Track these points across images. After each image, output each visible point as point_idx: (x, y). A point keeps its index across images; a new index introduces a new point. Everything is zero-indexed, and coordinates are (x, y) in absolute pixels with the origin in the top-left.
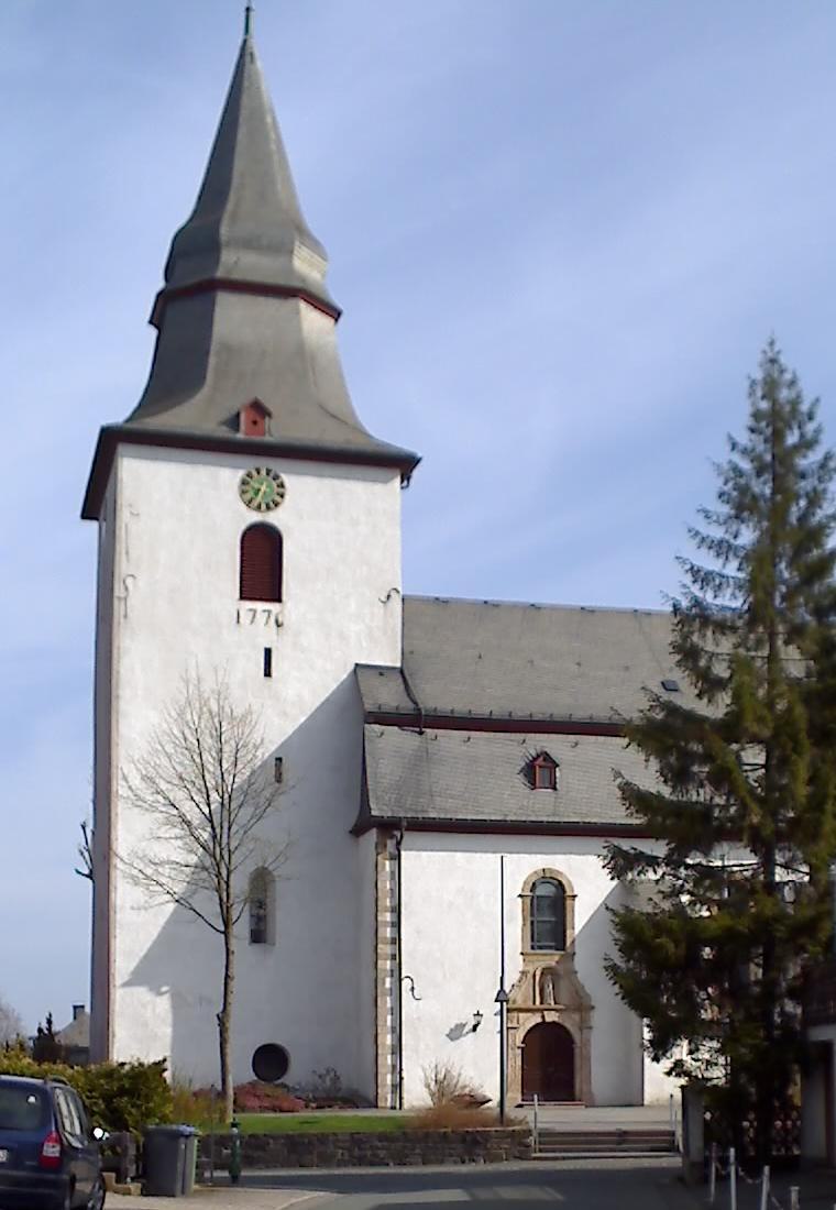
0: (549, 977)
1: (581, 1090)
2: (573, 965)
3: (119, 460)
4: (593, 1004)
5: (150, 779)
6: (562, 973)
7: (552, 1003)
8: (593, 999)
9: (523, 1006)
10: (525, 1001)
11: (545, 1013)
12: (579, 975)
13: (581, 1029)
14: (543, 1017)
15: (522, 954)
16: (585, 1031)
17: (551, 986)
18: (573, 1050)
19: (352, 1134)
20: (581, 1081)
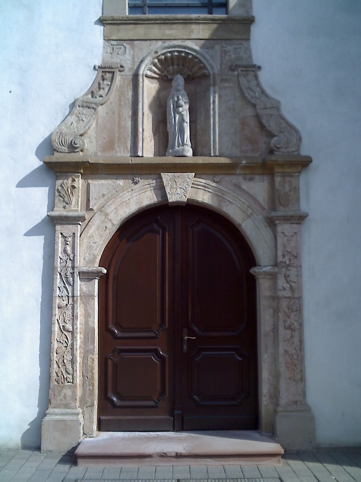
0: (179, 80)
1: (275, 396)
2: (248, 49)
3: (188, 101)
4: (305, 152)
5: (78, 117)
6: (216, 69)
7: (189, 152)
8: (305, 140)
9: (101, 158)
10: (109, 146)
11: (166, 177)
12: (263, 76)
13: (271, 223)
14: (161, 189)
15: (101, 21)
16: (284, 228)
17: (185, 109)
18: (252, 281)
19: (301, 266)
20: (277, 376)
